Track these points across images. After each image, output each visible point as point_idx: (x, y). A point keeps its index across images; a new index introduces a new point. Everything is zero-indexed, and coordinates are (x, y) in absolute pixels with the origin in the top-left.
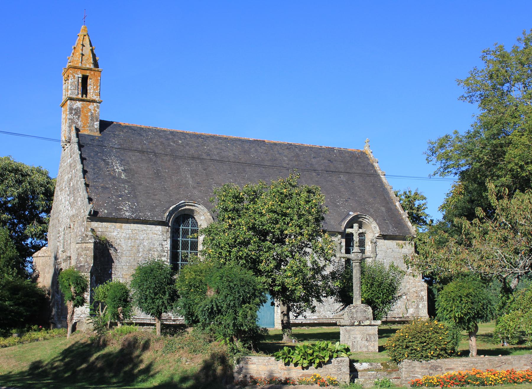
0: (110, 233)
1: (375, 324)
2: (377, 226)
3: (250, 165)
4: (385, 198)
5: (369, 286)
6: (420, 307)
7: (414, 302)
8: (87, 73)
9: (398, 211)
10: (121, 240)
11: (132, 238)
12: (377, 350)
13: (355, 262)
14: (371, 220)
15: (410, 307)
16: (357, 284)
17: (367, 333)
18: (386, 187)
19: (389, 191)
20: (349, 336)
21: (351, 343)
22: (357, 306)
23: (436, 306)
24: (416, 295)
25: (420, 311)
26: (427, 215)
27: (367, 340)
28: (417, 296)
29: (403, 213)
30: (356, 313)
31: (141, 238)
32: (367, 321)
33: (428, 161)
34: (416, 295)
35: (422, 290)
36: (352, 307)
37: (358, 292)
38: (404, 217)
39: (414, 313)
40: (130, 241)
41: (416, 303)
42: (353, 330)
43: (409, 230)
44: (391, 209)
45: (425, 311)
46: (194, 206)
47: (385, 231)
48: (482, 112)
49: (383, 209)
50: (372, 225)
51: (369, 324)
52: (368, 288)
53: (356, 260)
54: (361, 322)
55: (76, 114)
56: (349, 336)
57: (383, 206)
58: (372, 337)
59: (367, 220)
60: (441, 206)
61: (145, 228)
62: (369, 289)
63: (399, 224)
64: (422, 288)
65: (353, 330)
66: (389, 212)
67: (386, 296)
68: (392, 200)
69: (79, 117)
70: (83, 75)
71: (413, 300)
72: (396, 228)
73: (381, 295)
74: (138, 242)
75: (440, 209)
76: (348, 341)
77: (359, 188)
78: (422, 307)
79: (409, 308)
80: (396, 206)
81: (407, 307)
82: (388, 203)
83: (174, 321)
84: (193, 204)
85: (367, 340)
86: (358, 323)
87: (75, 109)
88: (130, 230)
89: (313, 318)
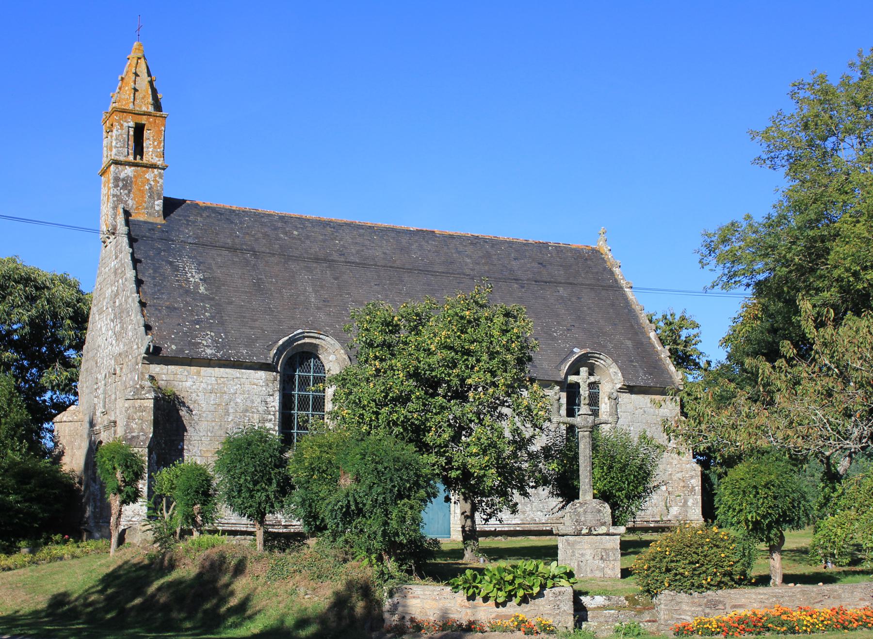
0: (180, 383)
1: (615, 532)
2: (619, 371)
3: (410, 271)
4: (632, 326)
5: (605, 470)
6: (690, 504)
7: (680, 496)
8: (143, 120)
9: (654, 347)
10: (199, 394)
11: (216, 391)
12: (619, 576)
13: (582, 430)
14: (609, 361)
15: (673, 504)
16: (586, 466)
17: (602, 547)
18: (633, 306)
19: (639, 314)
20: (573, 552)
21: (576, 564)
22: (586, 503)
23: (715, 503)
24: (682, 484)
25: (689, 510)
26: (701, 353)
27: (602, 559)
28: (684, 487)
29: (661, 350)
30: (585, 514)
31: (232, 391)
32: (603, 527)
33: (703, 264)
34: (682, 484)
35: (692, 477)
36: (578, 505)
37: (587, 480)
38: (662, 356)
39: (680, 514)
40: (213, 395)
41: (682, 497)
42: (579, 542)
43: (671, 377)
44: (642, 344)
45: (697, 511)
46: (319, 338)
47: (632, 380)
48: (791, 183)
49: (629, 343)
50: (611, 370)
51: (605, 532)
52: (604, 474)
53: (584, 427)
54: (592, 529)
55: (125, 187)
56: (573, 552)
57: (629, 339)
58: (611, 553)
59: (602, 362)
60: (724, 338)
61: (238, 375)
62: (606, 475)
63: (655, 368)
64: (693, 473)
65: (579, 542)
66: (638, 348)
67: (633, 486)
68: (644, 328)
69: (130, 192)
70: (136, 124)
71: (677, 493)
72: (650, 374)
73: (626, 485)
74: (226, 397)
75: (722, 344)
76: (571, 560)
77: (589, 308)
78: (693, 504)
79: (671, 506)
80: (650, 338)
81: (668, 505)
82: (636, 334)
83: (286, 527)
84: (316, 335)
85: (602, 559)
86: (587, 531)
87: (123, 180)
88: (214, 378)
89: (513, 522)
